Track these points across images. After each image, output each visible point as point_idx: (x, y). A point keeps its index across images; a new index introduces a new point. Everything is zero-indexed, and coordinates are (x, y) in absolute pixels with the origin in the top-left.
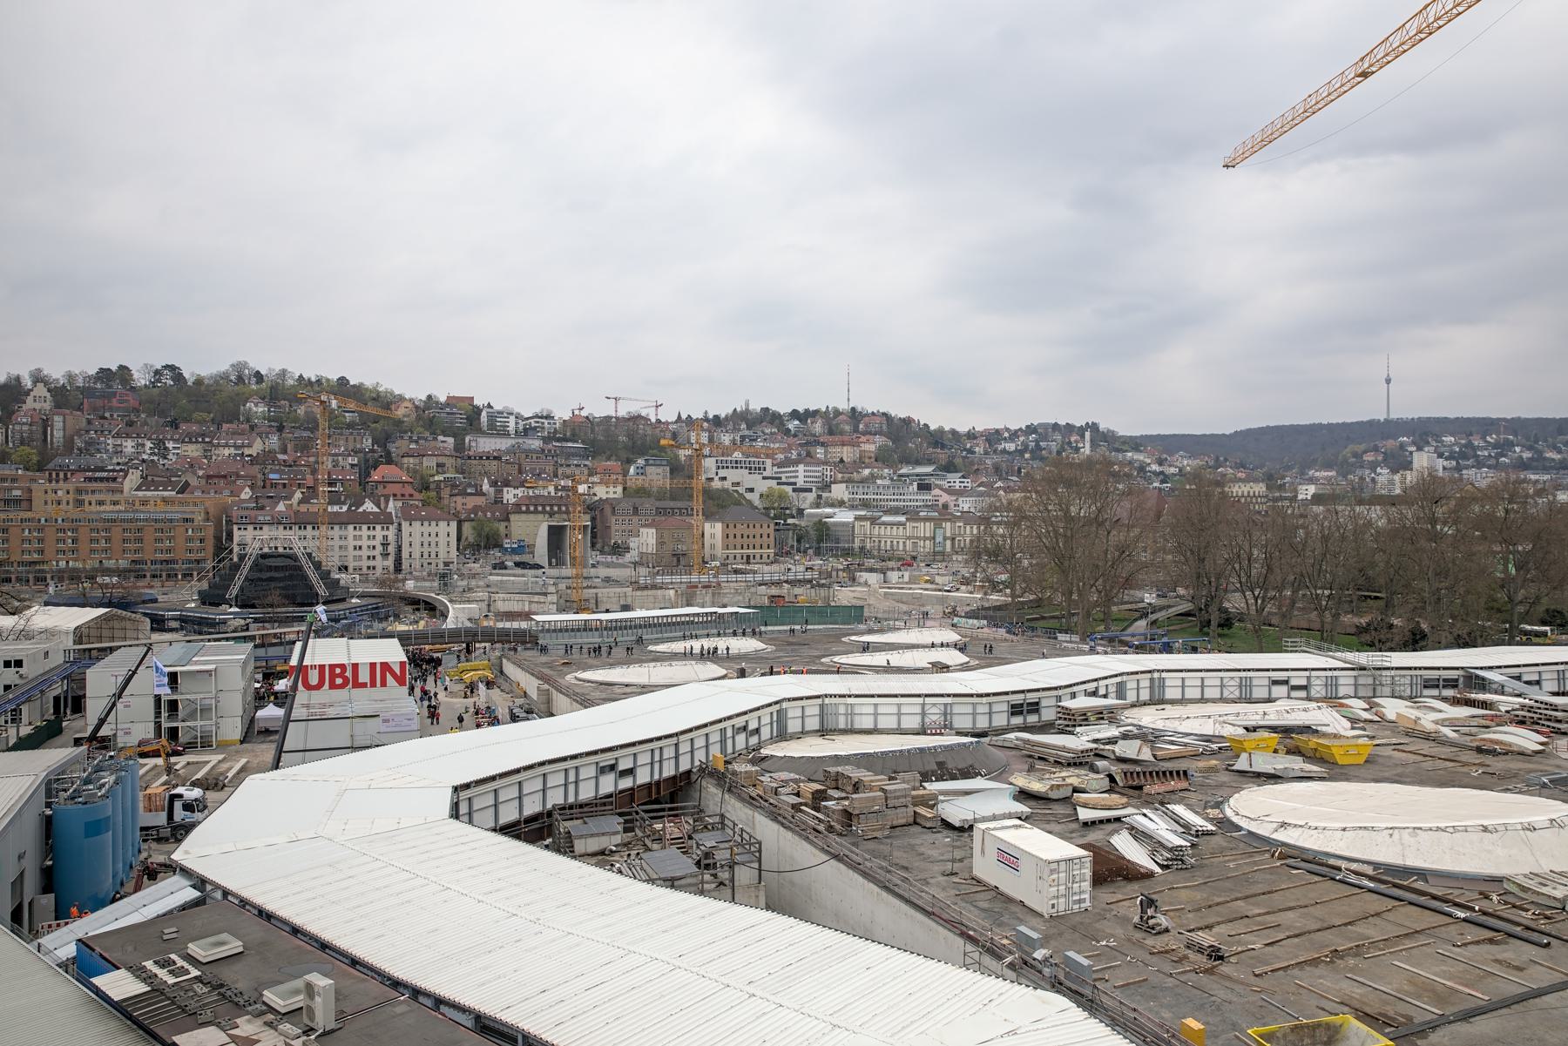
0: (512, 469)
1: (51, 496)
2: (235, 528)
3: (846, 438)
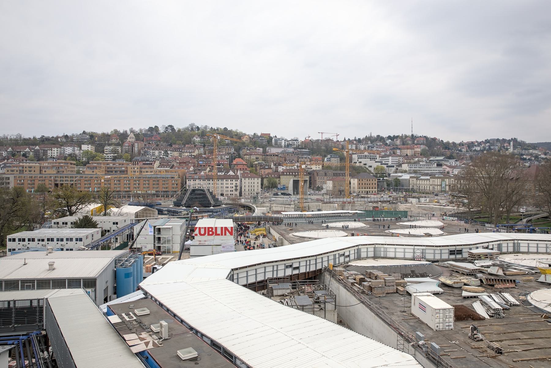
0: (283, 159)
1: (133, 170)
2: (187, 180)
3: (409, 146)
